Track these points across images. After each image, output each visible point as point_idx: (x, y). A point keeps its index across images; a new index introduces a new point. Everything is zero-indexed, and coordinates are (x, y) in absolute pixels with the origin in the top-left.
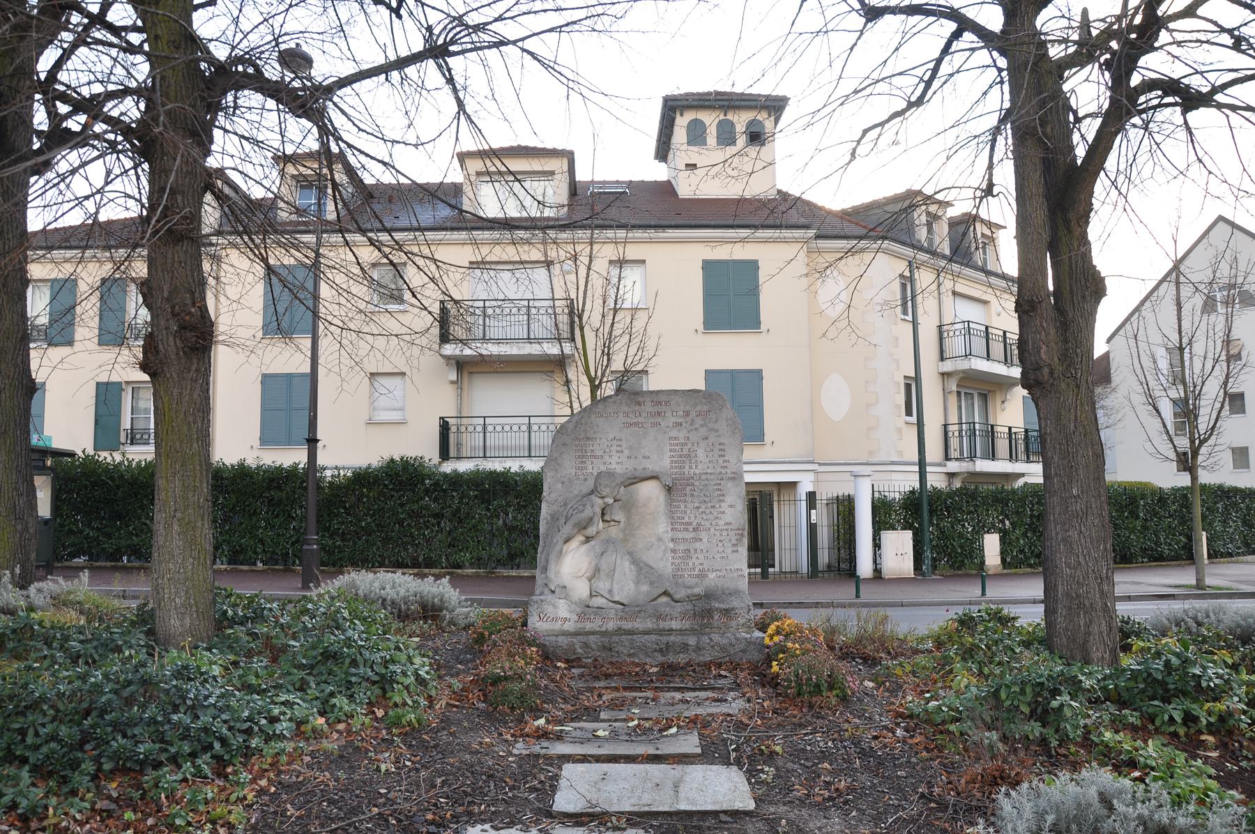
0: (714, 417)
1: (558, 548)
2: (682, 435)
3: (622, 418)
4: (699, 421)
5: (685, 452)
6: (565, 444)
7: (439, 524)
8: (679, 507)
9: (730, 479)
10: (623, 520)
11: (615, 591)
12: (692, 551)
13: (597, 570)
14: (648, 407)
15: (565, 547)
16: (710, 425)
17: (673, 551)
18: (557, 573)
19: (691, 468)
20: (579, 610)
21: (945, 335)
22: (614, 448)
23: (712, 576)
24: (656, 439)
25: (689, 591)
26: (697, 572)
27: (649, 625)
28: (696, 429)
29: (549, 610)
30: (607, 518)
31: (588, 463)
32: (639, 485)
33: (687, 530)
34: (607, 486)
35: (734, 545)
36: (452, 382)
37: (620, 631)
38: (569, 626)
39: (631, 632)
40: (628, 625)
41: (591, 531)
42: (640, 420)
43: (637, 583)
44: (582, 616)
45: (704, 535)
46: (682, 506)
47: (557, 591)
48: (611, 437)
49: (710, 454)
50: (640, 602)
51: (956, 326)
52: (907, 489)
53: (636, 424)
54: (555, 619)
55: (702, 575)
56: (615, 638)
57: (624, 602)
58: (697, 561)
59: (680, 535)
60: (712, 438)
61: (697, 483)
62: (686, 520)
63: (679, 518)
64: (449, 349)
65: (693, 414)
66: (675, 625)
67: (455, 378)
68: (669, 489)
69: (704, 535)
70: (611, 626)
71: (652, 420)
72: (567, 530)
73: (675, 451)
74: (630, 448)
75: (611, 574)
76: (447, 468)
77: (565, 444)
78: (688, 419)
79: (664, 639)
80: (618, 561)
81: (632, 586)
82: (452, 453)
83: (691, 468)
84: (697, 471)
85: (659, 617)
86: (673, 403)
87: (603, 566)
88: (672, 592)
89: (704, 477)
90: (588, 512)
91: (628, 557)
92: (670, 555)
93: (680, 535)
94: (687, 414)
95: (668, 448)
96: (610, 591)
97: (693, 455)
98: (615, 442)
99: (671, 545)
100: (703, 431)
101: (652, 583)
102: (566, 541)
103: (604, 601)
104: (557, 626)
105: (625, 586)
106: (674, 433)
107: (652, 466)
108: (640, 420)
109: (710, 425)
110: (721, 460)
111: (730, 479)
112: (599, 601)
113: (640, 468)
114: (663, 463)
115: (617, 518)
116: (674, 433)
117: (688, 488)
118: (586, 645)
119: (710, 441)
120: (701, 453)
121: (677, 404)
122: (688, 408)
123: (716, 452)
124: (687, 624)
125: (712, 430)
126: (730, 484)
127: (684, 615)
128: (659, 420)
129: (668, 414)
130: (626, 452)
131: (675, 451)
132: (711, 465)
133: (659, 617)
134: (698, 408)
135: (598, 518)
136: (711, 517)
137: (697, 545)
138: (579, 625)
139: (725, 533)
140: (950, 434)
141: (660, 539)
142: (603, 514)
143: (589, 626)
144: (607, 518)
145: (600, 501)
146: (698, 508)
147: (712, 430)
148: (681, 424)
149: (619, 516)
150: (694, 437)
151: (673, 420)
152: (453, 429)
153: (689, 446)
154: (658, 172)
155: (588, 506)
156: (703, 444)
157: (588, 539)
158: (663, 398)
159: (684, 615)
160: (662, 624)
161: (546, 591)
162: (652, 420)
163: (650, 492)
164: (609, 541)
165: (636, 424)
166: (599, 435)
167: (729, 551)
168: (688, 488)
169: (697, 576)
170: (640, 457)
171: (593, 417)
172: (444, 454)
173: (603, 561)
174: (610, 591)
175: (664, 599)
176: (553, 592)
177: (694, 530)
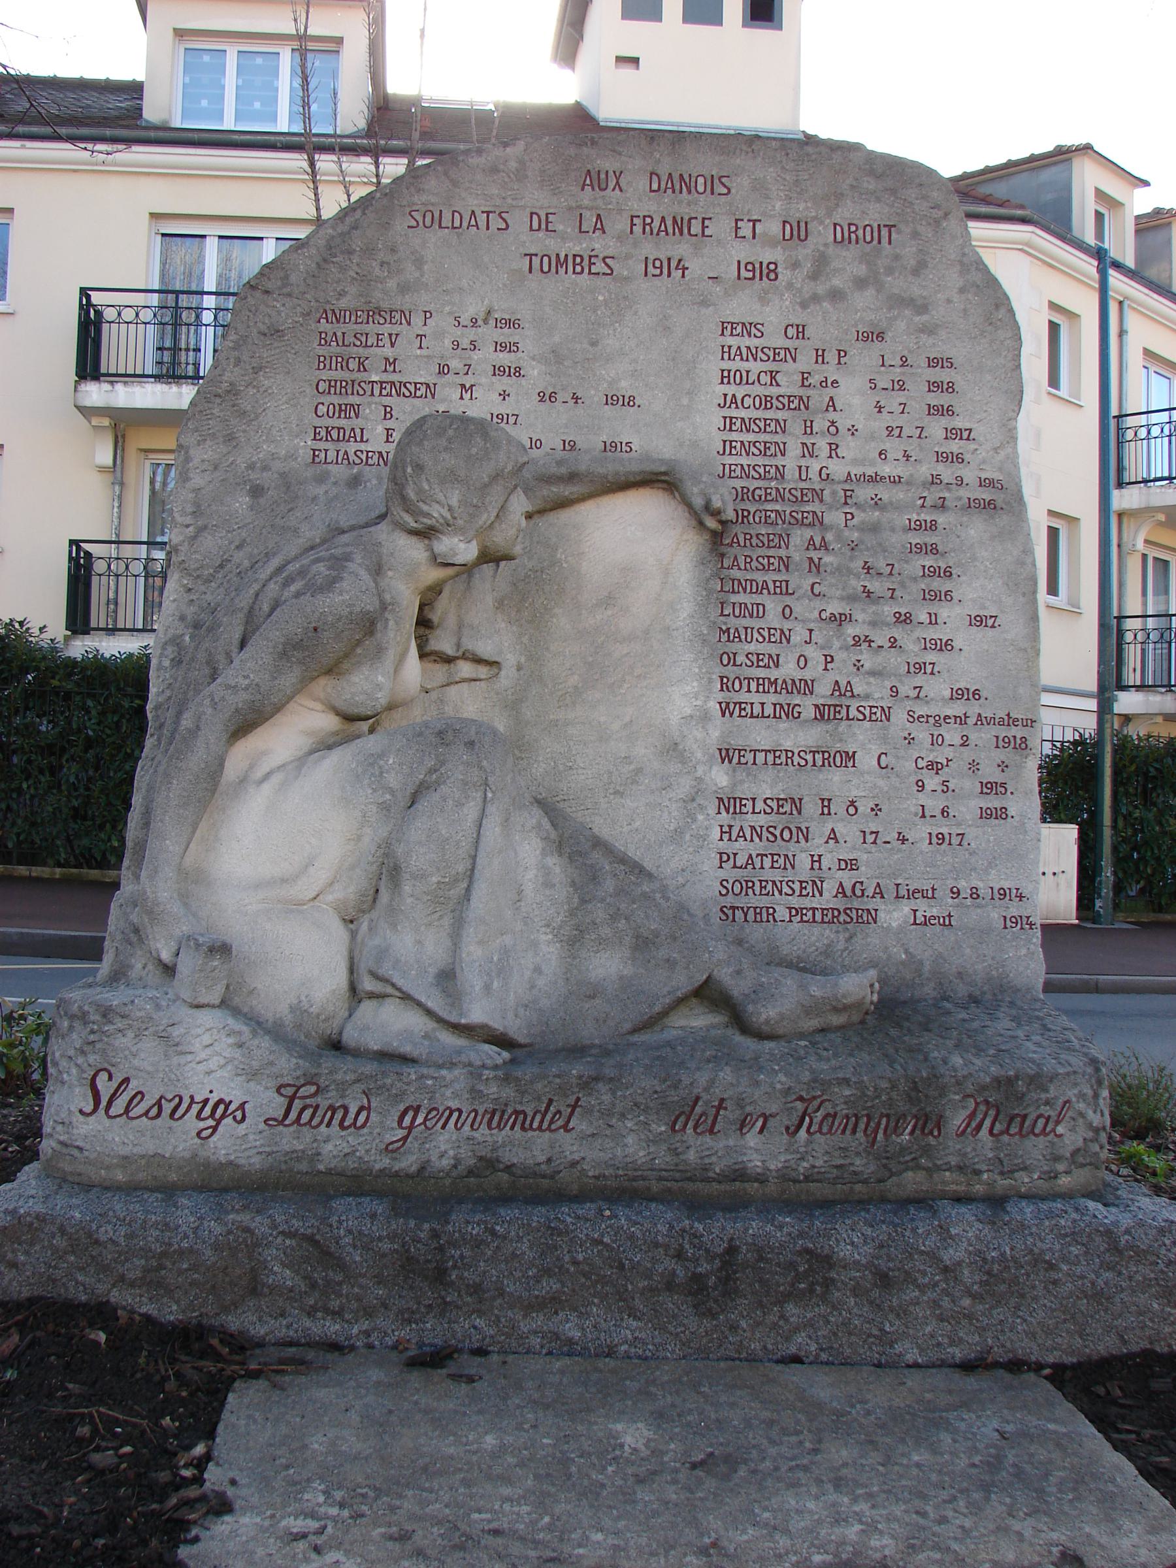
0: (909, 251)
1: (197, 758)
2: (773, 314)
3: (521, 237)
4: (848, 264)
5: (788, 385)
6: (275, 332)
7: (53, 770)
8: (758, 611)
9: (973, 505)
10: (510, 660)
11: (472, 979)
12: (811, 808)
13: (388, 871)
14: (637, 197)
15: (239, 756)
16: (896, 284)
17: (730, 803)
18: (193, 880)
19: (809, 451)
20: (288, 1065)
21: (1129, 435)
22: (486, 356)
23: (895, 915)
24: (664, 326)
25: (817, 988)
26: (828, 899)
27: (633, 1146)
28: (836, 295)
29: (141, 1060)
30: (443, 643)
31: (371, 411)
32: (588, 511)
33: (789, 713)
34: (450, 478)
35: (989, 788)
36: (102, 469)
37: (492, 1186)
38: (233, 1144)
39: (542, 1190)
40: (529, 1148)
41: (366, 684)
42: (600, 244)
43: (575, 938)
44: (299, 1102)
45: (861, 739)
46: (773, 618)
47: (186, 965)
48: (473, 308)
49: (892, 402)
50: (589, 1033)
51: (1155, 418)
52: (1069, 737)
53: (580, 263)
54: (170, 1108)
55: (853, 913)
56: (466, 1223)
57: (514, 1027)
58: (831, 850)
59: (760, 735)
60: (900, 339)
61: (835, 518)
62: (788, 669)
63: (757, 660)
64: (95, 394)
65: (822, 235)
66: (760, 1151)
67: (109, 461)
68: (718, 534)
69: (861, 739)
70: (445, 1148)
71: (649, 249)
72: (247, 671)
73: (744, 379)
74: (555, 358)
75: (455, 900)
76: (79, 648)
77: (275, 332)
78: (804, 252)
79: (718, 1230)
80: (492, 831)
81: (550, 952)
82: (98, 616)
83: (809, 451)
84: (838, 469)
85: (687, 1113)
86: (741, 185)
87: (419, 856)
88: (737, 988)
89: (864, 493)
90: (351, 593)
91: (536, 816)
92: (711, 822)
93: (760, 735)
94: (797, 232)
95: (713, 366)
96: (447, 977)
97: (819, 398)
98: (489, 334)
99: (720, 777)
100: (866, 306)
101: (643, 944)
102: (246, 723)
103: (415, 1021)
104: (179, 1139)
105: (516, 953)
106: (742, 306)
107: (647, 438)
108: (600, 244)
109: (896, 284)
110: (936, 428)
111: (973, 505)
112: (388, 1024)
113: (591, 442)
114: (689, 424)
115: (485, 649)
116: (742, 306)
117: (799, 537)
118: (319, 1251)
119: (893, 348)
120: (853, 397)
121: (759, 187)
122: (801, 209)
123: (918, 396)
124: (818, 1151)
125: (901, 302)
126: (976, 529)
127: (806, 1110)
128: (679, 248)
129: (720, 227)
130: (534, 371)
131: (744, 379)
132: (894, 448)
133: (687, 1113)
134: (846, 212)
135: (399, 632)
136: (894, 660)
137: (834, 781)
138: (289, 1140)
139: (952, 735)
140: (1129, 637)
141: (673, 749)
142: (424, 623)
143: (334, 1146)
144: (443, 643)
145: (413, 551)
146: (840, 620)
147: (901, 302)
148: (769, 272)
149: (495, 637)
150: (825, 326)
151: (741, 252)
152: (99, 567)
153: (805, 361)
154: (558, 88)
155: (358, 567)
156: (864, 358)
157: (355, 721)
158: (701, 164)
159: (806, 1110)
160: (697, 1148)
161: (138, 965)
162: (649, 249)
163: (634, 545)
164: (447, 735)
165: (580, 263)
166: (424, 300)
167: (968, 808)
168: (799, 537)
169: (830, 917)
170: (594, 395)
171: (401, 224)
172: (79, 618)
173: (419, 827)
174: (447, 977)
175: (699, 1020)
176: (169, 970)
177: (822, 714)
